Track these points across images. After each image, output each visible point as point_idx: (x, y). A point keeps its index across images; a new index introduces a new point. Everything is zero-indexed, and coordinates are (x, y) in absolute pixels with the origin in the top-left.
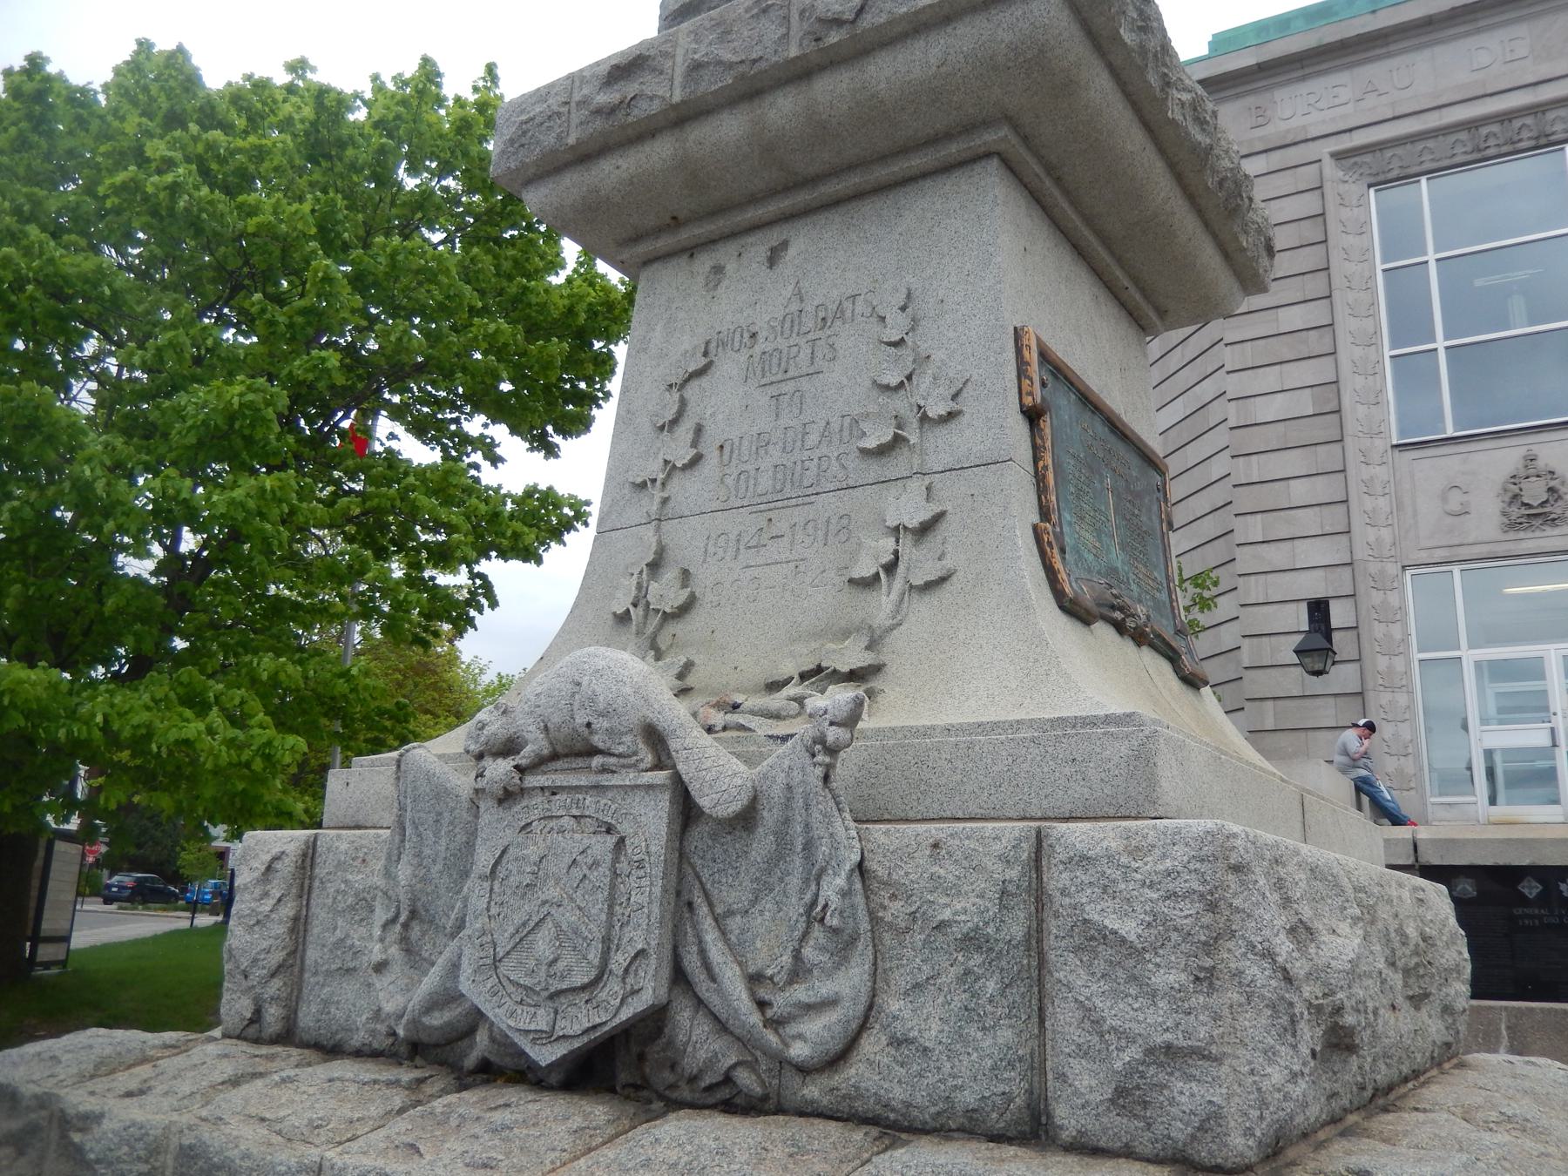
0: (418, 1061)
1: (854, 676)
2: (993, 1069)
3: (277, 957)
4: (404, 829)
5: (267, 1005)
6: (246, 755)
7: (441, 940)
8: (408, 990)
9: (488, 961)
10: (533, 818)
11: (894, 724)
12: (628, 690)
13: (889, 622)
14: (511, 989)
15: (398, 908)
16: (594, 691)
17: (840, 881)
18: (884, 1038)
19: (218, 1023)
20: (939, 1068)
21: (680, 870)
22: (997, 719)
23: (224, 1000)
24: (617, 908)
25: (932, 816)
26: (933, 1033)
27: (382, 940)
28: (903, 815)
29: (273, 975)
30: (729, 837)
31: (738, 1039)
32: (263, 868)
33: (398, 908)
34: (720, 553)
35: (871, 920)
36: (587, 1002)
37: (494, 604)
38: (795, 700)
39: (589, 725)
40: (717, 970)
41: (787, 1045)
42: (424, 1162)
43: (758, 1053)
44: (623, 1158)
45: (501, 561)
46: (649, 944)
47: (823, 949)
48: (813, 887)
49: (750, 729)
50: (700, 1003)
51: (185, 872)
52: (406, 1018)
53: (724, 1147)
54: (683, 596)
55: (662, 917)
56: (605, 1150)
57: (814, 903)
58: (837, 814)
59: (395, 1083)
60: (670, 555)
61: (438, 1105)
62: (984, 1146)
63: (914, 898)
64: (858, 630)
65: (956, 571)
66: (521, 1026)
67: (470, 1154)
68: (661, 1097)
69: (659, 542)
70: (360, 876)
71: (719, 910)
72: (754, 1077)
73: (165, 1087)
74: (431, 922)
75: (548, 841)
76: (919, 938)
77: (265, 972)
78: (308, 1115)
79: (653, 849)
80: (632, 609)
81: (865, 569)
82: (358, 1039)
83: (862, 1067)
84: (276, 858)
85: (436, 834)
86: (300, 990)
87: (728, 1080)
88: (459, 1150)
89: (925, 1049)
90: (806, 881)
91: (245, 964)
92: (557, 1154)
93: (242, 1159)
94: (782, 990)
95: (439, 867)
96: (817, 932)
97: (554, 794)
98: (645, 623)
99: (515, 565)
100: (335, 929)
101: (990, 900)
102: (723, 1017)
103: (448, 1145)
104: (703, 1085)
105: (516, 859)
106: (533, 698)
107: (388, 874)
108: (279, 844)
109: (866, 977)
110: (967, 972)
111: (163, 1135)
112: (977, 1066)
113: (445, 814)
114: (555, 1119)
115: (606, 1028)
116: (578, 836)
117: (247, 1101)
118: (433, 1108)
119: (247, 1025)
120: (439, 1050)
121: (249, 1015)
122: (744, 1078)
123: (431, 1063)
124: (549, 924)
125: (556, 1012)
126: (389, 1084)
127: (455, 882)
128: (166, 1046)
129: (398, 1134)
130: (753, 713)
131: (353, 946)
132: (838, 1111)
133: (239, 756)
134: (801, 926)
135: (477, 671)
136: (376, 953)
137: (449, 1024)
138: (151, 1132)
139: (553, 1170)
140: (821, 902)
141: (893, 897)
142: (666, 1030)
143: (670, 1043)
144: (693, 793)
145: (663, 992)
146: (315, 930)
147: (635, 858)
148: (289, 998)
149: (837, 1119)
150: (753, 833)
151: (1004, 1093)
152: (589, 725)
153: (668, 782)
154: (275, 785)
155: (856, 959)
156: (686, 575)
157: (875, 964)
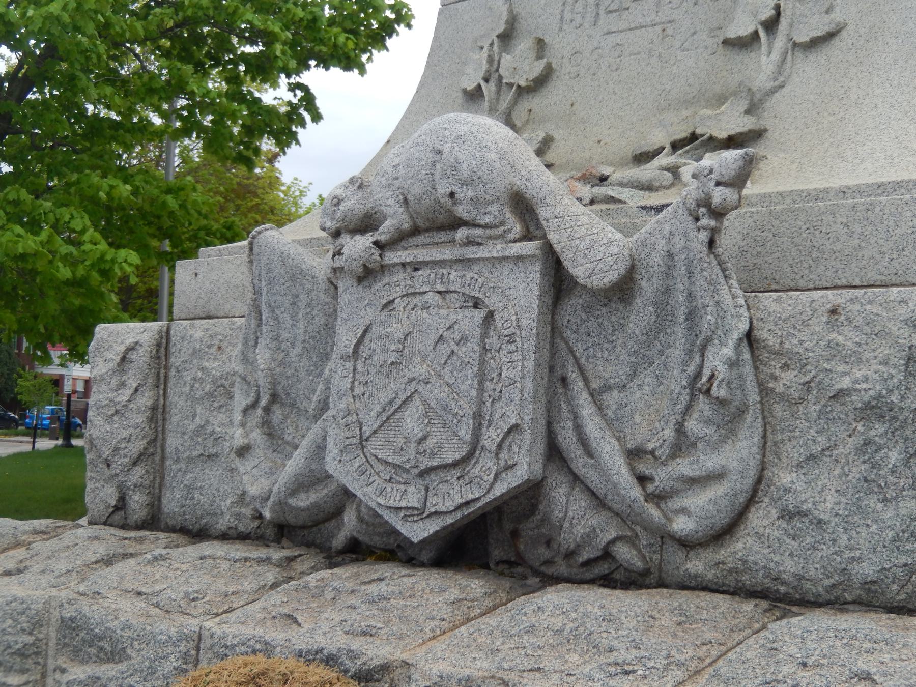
0: (285, 542)
1: (731, 142)
2: (894, 540)
3: (137, 446)
4: (260, 314)
5: (131, 493)
6: (81, 271)
7: (303, 423)
8: (273, 474)
9: (355, 441)
10: (395, 295)
11: (781, 189)
12: (493, 156)
13: (770, 85)
14: (379, 467)
15: (258, 394)
16: (456, 159)
17: (728, 351)
18: (774, 511)
19: (83, 513)
20: (835, 541)
21: (552, 345)
22: (899, 179)
23: (88, 489)
24: (488, 383)
25: (825, 284)
26: (829, 505)
27: (243, 425)
28: (792, 284)
29: (135, 464)
30: (604, 310)
31: (617, 514)
32: (118, 359)
33: (258, 394)
34: (578, 19)
35: (761, 392)
36: (458, 479)
37: (317, 117)
38: (668, 169)
39: (452, 195)
40: (594, 445)
41: (669, 520)
42: (302, 630)
43: (638, 529)
44: (506, 624)
45: (321, 70)
46: (522, 419)
47: (708, 422)
48: (697, 359)
49: (620, 201)
50: (576, 479)
51: (23, 398)
52: (272, 500)
53: (610, 614)
54: (538, 68)
55: (536, 391)
56: (485, 619)
57: (698, 375)
58: (723, 281)
59: (268, 560)
60: (523, 24)
61: (312, 579)
62: (885, 616)
63: (809, 367)
64: (734, 94)
65: (846, 25)
66: (392, 503)
67: (349, 623)
68: (536, 573)
69: (511, 11)
70: (217, 364)
71: (595, 385)
72: (635, 552)
73: (41, 567)
74: (293, 406)
75: (413, 318)
76: (814, 409)
77: (127, 460)
78: (184, 588)
79: (524, 322)
80: (483, 84)
81: (742, 27)
82: (223, 523)
83: (750, 541)
84: (131, 349)
85: (293, 317)
86: (163, 478)
87: (607, 554)
88: (338, 619)
89: (820, 522)
90: (689, 353)
91: (106, 453)
92: (437, 623)
93: (123, 629)
94: (664, 464)
95: (298, 350)
96: (702, 404)
97: (416, 270)
98: (498, 99)
99: (336, 71)
100: (194, 416)
101: (895, 366)
102: (601, 492)
103: (326, 615)
104: (581, 560)
105: (380, 338)
106: (390, 170)
107: (245, 359)
108: (132, 335)
109: (755, 449)
110: (867, 443)
111: (44, 609)
112: (876, 537)
113: (302, 296)
114: (431, 591)
115: (480, 504)
116: (443, 312)
117: (122, 578)
118: (307, 583)
119: (113, 513)
120: (306, 532)
121: (113, 503)
122: (624, 552)
123: (299, 544)
124: (417, 401)
125: (427, 489)
126: (260, 561)
127: (315, 365)
128: (36, 532)
129: (274, 605)
130: (621, 184)
131: (213, 432)
132: (724, 584)
133: (73, 273)
134: (685, 398)
135: (297, 193)
136: (238, 437)
137: (316, 505)
138: (32, 606)
139: (434, 638)
140: (706, 373)
141: (785, 367)
142: (541, 507)
143: (545, 520)
144: (565, 263)
145: (538, 467)
146: (174, 418)
147: (506, 332)
148: (151, 485)
149: (723, 592)
150: (630, 304)
151: (906, 565)
152: (452, 195)
153: (538, 252)
154: (111, 300)
155: (743, 432)
156: (541, 44)
157: (764, 437)
